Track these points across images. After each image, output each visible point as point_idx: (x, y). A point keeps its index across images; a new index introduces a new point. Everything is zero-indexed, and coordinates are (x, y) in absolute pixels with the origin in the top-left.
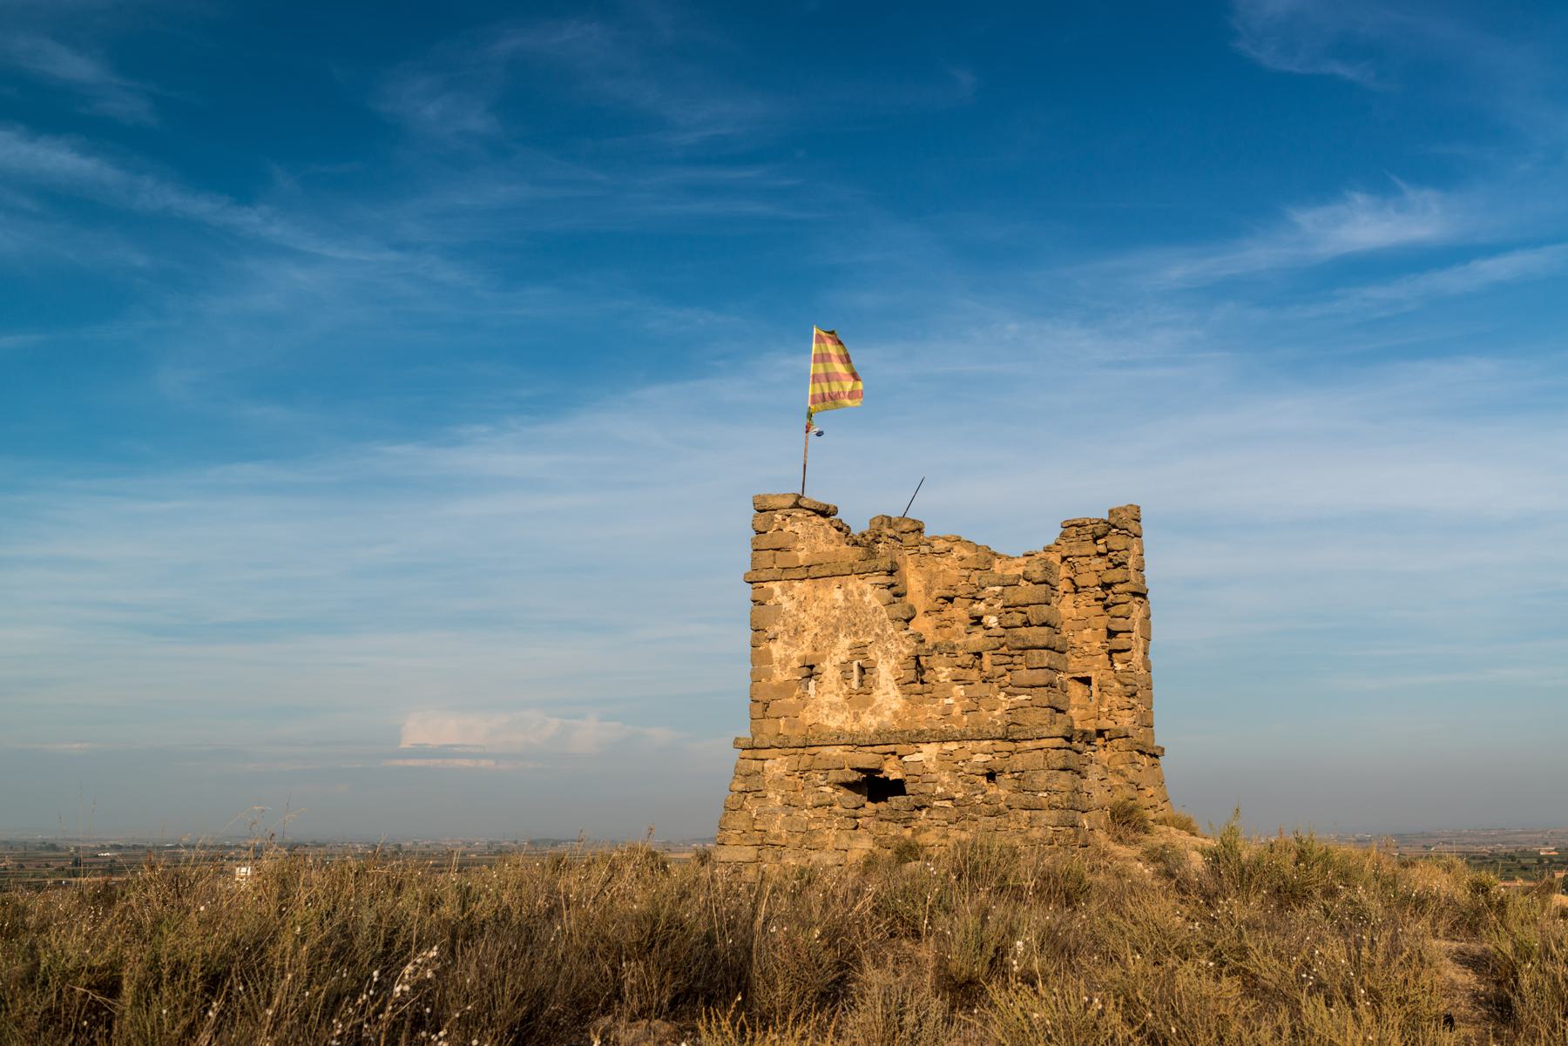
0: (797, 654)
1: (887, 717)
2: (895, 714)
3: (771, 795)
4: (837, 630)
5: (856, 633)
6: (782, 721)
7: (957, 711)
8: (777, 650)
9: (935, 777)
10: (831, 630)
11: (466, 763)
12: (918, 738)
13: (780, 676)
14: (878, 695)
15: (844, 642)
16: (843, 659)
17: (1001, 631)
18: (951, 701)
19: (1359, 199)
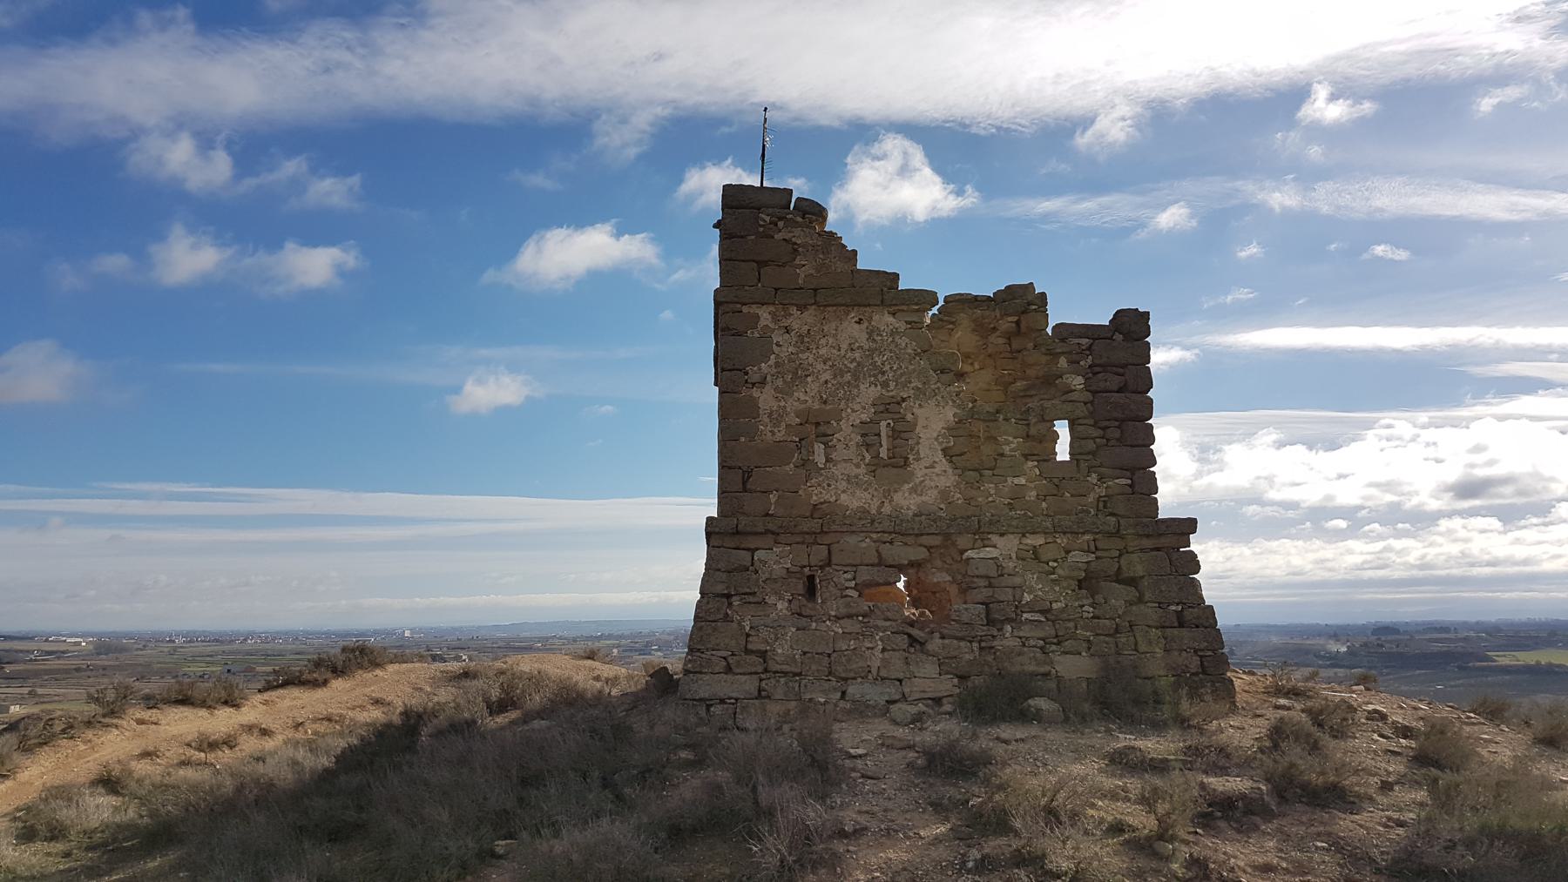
0: (791, 405)
1: (930, 497)
3: (771, 600)
4: (857, 379)
5: (885, 385)
6: (773, 498)
7: (1032, 495)
8: (766, 399)
9: (1017, 580)
10: (848, 377)
12: (981, 533)
14: (919, 470)
15: (869, 392)
16: (864, 417)
17: (1089, 396)
18: (1023, 481)
19: (886, 223)
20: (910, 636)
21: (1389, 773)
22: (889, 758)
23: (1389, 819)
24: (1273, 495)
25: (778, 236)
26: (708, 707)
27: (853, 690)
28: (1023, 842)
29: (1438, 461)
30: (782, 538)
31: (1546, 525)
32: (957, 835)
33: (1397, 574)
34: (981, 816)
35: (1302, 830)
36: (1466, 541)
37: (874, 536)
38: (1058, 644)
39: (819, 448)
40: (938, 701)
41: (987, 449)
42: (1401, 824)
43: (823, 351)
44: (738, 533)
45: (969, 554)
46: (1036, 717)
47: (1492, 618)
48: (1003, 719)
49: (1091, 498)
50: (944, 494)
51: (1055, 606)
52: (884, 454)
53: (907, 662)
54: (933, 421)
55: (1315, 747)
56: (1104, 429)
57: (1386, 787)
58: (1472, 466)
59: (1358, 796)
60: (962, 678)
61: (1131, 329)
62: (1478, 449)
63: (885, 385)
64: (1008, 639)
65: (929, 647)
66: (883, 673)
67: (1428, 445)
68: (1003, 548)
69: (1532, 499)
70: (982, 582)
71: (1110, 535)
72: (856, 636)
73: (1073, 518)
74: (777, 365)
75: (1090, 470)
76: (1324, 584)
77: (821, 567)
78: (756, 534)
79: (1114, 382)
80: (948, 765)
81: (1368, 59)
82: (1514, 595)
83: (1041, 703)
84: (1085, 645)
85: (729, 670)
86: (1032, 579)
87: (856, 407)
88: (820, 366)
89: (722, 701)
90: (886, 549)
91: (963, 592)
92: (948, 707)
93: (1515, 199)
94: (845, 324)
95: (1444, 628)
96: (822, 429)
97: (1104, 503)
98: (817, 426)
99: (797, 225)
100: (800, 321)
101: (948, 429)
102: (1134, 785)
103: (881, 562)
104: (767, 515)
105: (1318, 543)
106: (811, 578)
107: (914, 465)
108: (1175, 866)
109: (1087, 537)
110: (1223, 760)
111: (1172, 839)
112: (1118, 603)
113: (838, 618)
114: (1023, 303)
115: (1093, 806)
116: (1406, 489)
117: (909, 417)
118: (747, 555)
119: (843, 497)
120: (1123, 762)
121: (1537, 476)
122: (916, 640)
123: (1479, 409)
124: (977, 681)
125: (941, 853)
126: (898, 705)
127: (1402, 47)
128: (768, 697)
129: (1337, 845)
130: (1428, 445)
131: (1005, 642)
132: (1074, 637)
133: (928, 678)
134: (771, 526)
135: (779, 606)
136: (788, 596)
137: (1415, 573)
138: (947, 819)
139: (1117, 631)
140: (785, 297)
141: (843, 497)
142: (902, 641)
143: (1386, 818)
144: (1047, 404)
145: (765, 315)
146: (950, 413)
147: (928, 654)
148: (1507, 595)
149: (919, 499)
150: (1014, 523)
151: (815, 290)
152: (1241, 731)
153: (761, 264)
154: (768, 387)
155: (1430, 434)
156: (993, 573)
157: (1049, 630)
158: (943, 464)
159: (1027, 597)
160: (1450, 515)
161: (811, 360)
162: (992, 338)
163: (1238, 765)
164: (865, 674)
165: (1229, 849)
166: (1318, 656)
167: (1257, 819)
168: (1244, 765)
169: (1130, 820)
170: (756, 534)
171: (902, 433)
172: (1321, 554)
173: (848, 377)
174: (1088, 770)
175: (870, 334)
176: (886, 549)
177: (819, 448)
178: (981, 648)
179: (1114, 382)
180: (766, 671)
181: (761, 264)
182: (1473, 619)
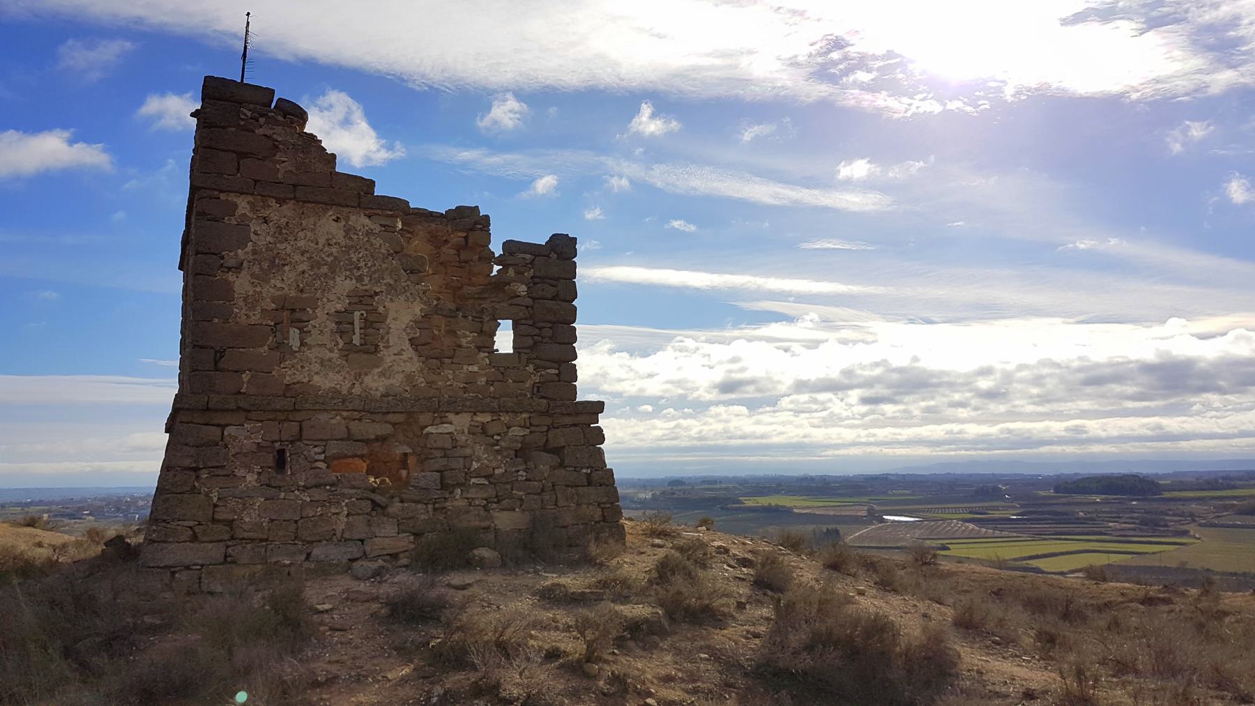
0: (268, 291)
1: (397, 381)
2: (409, 378)
3: (240, 472)
6: (246, 377)
7: (482, 381)
8: (242, 284)
9: (468, 451)
12: (439, 412)
14: (387, 356)
15: (344, 285)
16: (339, 307)
17: (529, 302)
18: (476, 369)
20: (373, 501)
21: (741, 595)
22: (354, 610)
23: (748, 632)
24: (606, 387)
25: (259, 131)
26: (173, 573)
27: (317, 551)
28: (480, 675)
29: (711, 368)
30: (253, 415)
31: (774, 412)
32: (422, 675)
33: (684, 444)
34: (441, 655)
35: (688, 645)
36: (727, 421)
37: (345, 414)
38: (498, 502)
39: (294, 334)
40: (394, 556)
41: (448, 341)
42: (756, 636)
43: (301, 243)
44: (208, 409)
45: (429, 429)
46: (482, 564)
47: (742, 474)
48: (453, 568)
49: (528, 384)
50: (409, 378)
51: (497, 472)
52: (356, 340)
53: (369, 524)
54: (402, 315)
55: (689, 575)
56: (540, 329)
57: (741, 606)
58: (730, 371)
59: (724, 615)
60: (416, 535)
61: (562, 250)
62: (735, 360)
63: (360, 279)
64: (458, 500)
65: (390, 510)
66: (347, 535)
67: (704, 356)
68: (459, 423)
69: (767, 394)
70: (438, 454)
71: (542, 414)
72: (322, 503)
73: (515, 400)
74: (254, 252)
75: (529, 361)
76: (637, 450)
77: (292, 442)
78: (227, 410)
79: (550, 291)
80: (410, 612)
81: (695, 79)
82: (755, 458)
83: (484, 552)
84: (518, 503)
85: (194, 538)
86: (480, 450)
87: (331, 297)
88: (297, 257)
89: (188, 568)
90: (354, 426)
91: (421, 462)
92: (404, 561)
93: (778, 190)
94: (323, 221)
95: (714, 481)
96: (297, 315)
97: (538, 389)
98: (292, 312)
99: (277, 123)
100: (280, 213)
101: (415, 322)
102: (564, 616)
103: (349, 437)
104: (239, 393)
105: (633, 421)
106: (281, 453)
107: (384, 352)
108: (601, 683)
109: (525, 415)
110: (623, 591)
111: (599, 660)
112: (544, 468)
113: (306, 488)
114: (471, 223)
115: (532, 637)
116: (689, 385)
117: (381, 309)
118: (218, 431)
119: (316, 378)
120: (551, 597)
121: (769, 379)
122: (379, 505)
123: (736, 333)
124: (430, 537)
125: (408, 691)
126: (360, 563)
127: (717, 74)
128: (234, 562)
129: (716, 655)
130: (704, 356)
131: (456, 503)
132: (511, 497)
133: (388, 537)
134: (242, 404)
135: (249, 478)
136: (257, 469)
137: (695, 442)
138: (411, 661)
139: (543, 490)
140: (262, 188)
141: (316, 378)
142: (366, 506)
143: (745, 631)
144: (498, 306)
145: (243, 205)
146: (417, 309)
147: (388, 516)
148: (751, 459)
149: (387, 382)
150: (468, 403)
151: (294, 186)
152: (635, 564)
153: (242, 155)
154: (244, 273)
155: (707, 348)
156: (448, 445)
157: (491, 492)
158: (409, 352)
159: (475, 465)
160: (717, 404)
161: (288, 250)
162: (445, 249)
163: (636, 594)
164: (330, 538)
165: (639, 665)
166: (632, 501)
167: (656, 638)
168: (642, 595)
169: (562, 646)
170: (227, 410)
171: (374, 322)
172: (637, 429)
173: (325, 269)
174: (523, 605)
175: (347, 232)
176: (354, 426)
177: (294, 334)
178: (435, 509)
179: (550, 291)
180: (232, 538)
181: (242, 155)
182: (731, 475)
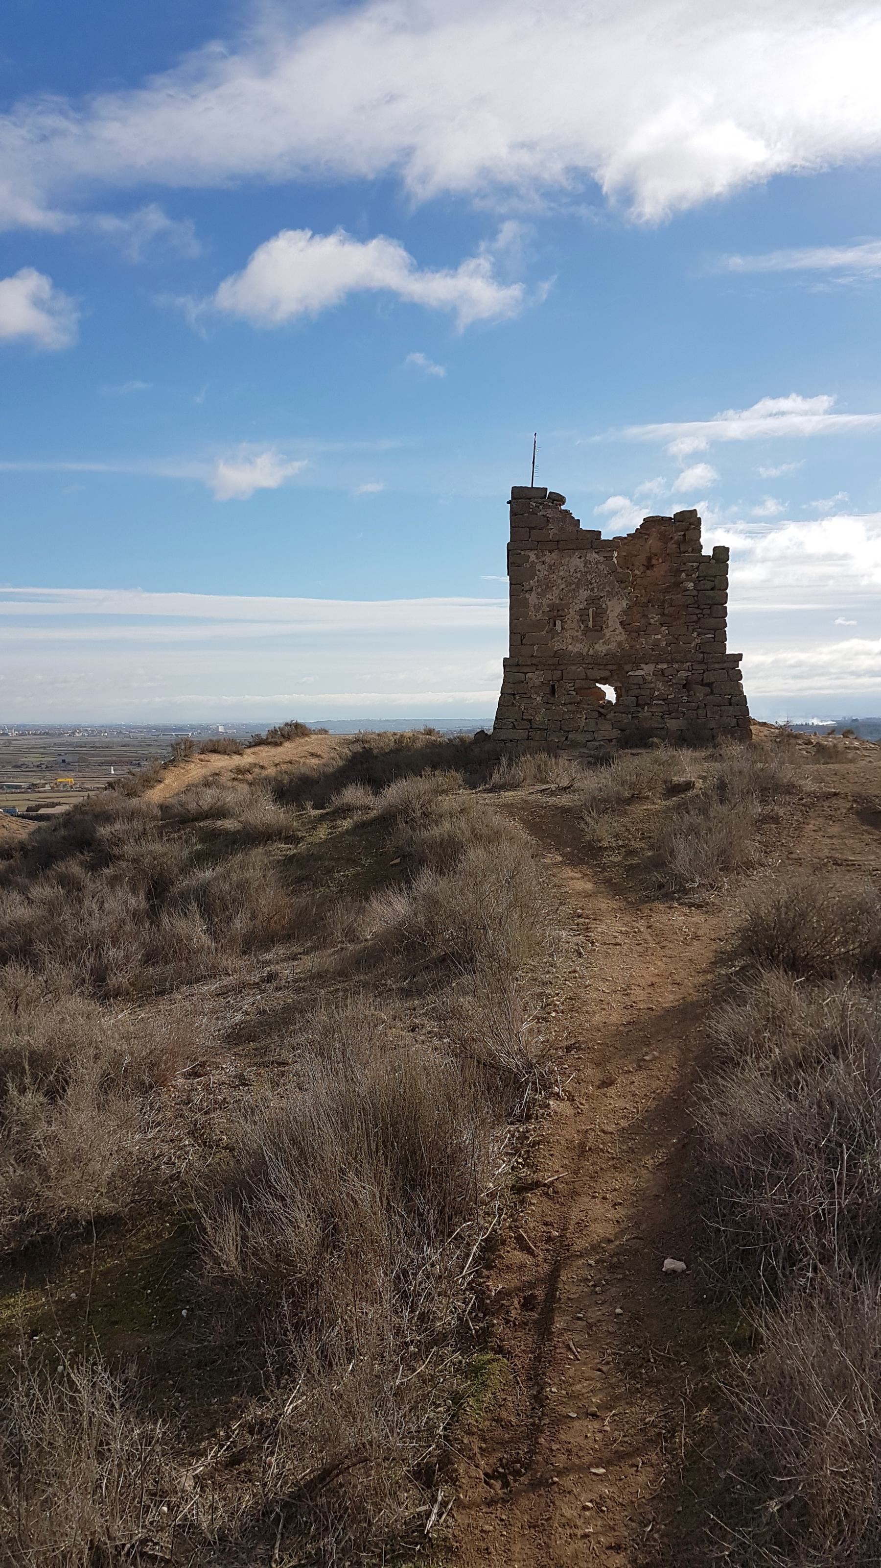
0: (545, 601)
1: (613, 646)
4: (578, 587)
5: (592, 590)
6: (535, 648)
9: (653, 685)
11: (866, 680)
13: (534, 615)
14: (607, 633)
15: (584, 594)
17: (695, 593)
18: (659, 637)
